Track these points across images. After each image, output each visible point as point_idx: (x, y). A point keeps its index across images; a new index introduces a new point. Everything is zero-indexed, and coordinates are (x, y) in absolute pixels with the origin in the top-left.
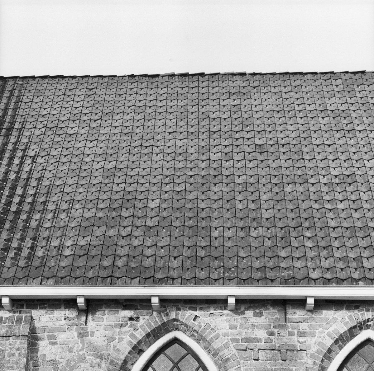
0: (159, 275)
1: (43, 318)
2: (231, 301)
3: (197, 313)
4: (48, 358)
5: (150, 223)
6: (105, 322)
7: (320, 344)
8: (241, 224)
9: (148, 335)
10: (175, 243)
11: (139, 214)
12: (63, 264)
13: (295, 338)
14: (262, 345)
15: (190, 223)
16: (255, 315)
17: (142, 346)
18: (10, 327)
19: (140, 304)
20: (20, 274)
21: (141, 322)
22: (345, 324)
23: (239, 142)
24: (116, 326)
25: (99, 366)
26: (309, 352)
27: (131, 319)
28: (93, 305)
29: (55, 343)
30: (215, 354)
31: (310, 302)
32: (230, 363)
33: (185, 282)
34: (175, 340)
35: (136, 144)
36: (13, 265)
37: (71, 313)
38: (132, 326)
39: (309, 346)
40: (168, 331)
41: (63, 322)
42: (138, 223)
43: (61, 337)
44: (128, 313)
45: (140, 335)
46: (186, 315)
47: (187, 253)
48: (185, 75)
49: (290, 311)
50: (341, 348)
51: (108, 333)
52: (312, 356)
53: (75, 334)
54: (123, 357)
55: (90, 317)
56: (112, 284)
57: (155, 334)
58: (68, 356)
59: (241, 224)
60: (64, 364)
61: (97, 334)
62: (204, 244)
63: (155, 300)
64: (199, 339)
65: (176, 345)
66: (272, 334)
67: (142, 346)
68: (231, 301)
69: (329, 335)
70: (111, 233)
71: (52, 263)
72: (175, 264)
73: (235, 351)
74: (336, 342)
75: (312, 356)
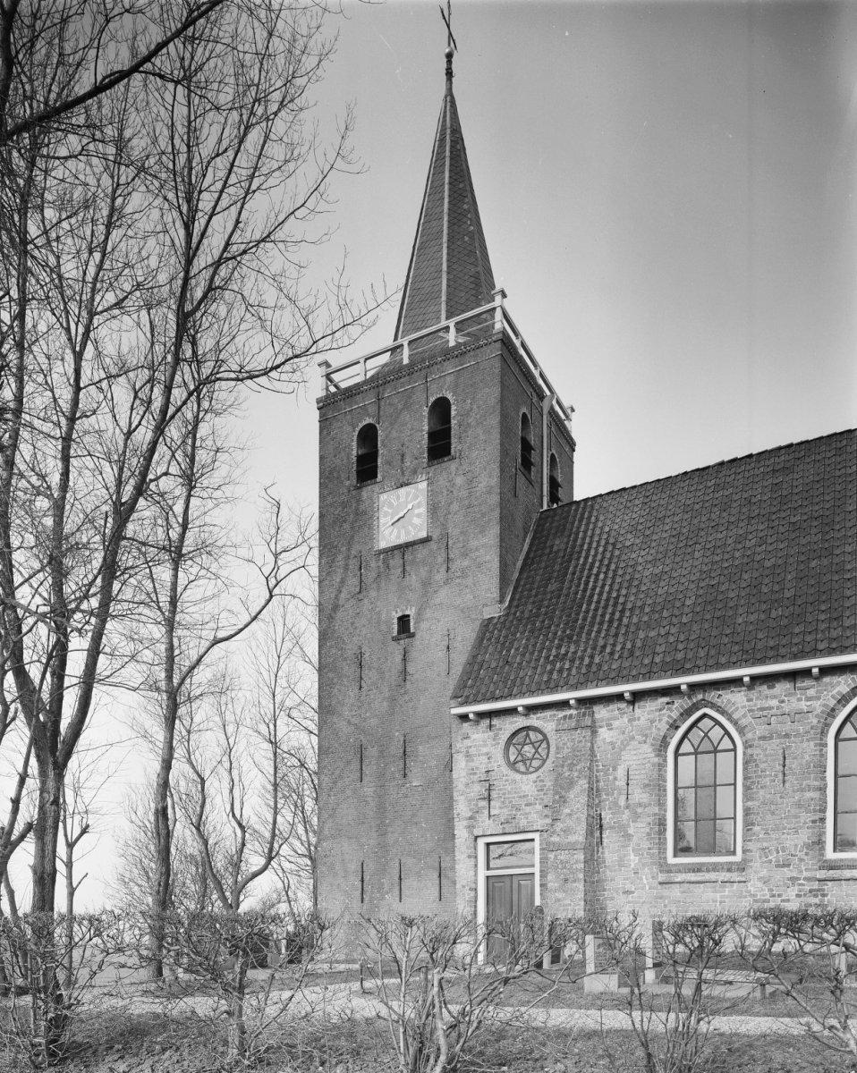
0: (688, 666)
1: (601, 712)
2: (746, 679)
3: (720, 693)
4: (608, 740)
5: (685, 620)
6: (648, 709)
7: (825, 705)
8: (764, 607)
9: (682, 715)
10: (704, 634)
11: (676, 612)
12: (614, 667)
13: (803, 703)
14: (774, 711)
15: (718, 614)
16: (769, 688)
17: (678, 723)
18: (578, 721)
19: (673, 691)
20: (582, 680)
21: (676, 705)
22: (848, 685)
23: (777, 522)
24: (656, 710)
25: (645, 742)
26: (815, 713)
27: (668, 703)
28: (637, 696)
29: (611, 729)
30: (735, 723)
31: (815, 671)
32: (747, 729)
33: (708, 669)
34: (705, 716)
35: (681, 545)
36: (578, 673)
37: (623, 705)
38: (669, 709)
39: (815, 708)
40: (698, 709)
41: (617, 712)
42: (675, 620)
43: (616, 724)
44: (666, 700)
45: (675, 715)
46: (712, 695)
47: (713, 642)
48: (734, 460)
49: (596, 708)
50: (844, 706)
51: (651, 716)
52: (817, 716)
53: (626, 720)
54: (662, 734)
55: (637, 705)
56: (650, 679)
57: (688, 713)
58: (622, 737)
59: (764, 607)
60: (619, 743)
61: (642, 718)
62: (728, 632)
63: (684, 687)
64: (723, 712)
65: (706, 720)
66: (783, 702)
67: (678, 723)
68: (746, 679)
69: (833, 697)
70: (652, 634)
71: (605, 667)
72: (702, 653)
73: (751, 719)
74: (839, 702)
75: (817, 716)
